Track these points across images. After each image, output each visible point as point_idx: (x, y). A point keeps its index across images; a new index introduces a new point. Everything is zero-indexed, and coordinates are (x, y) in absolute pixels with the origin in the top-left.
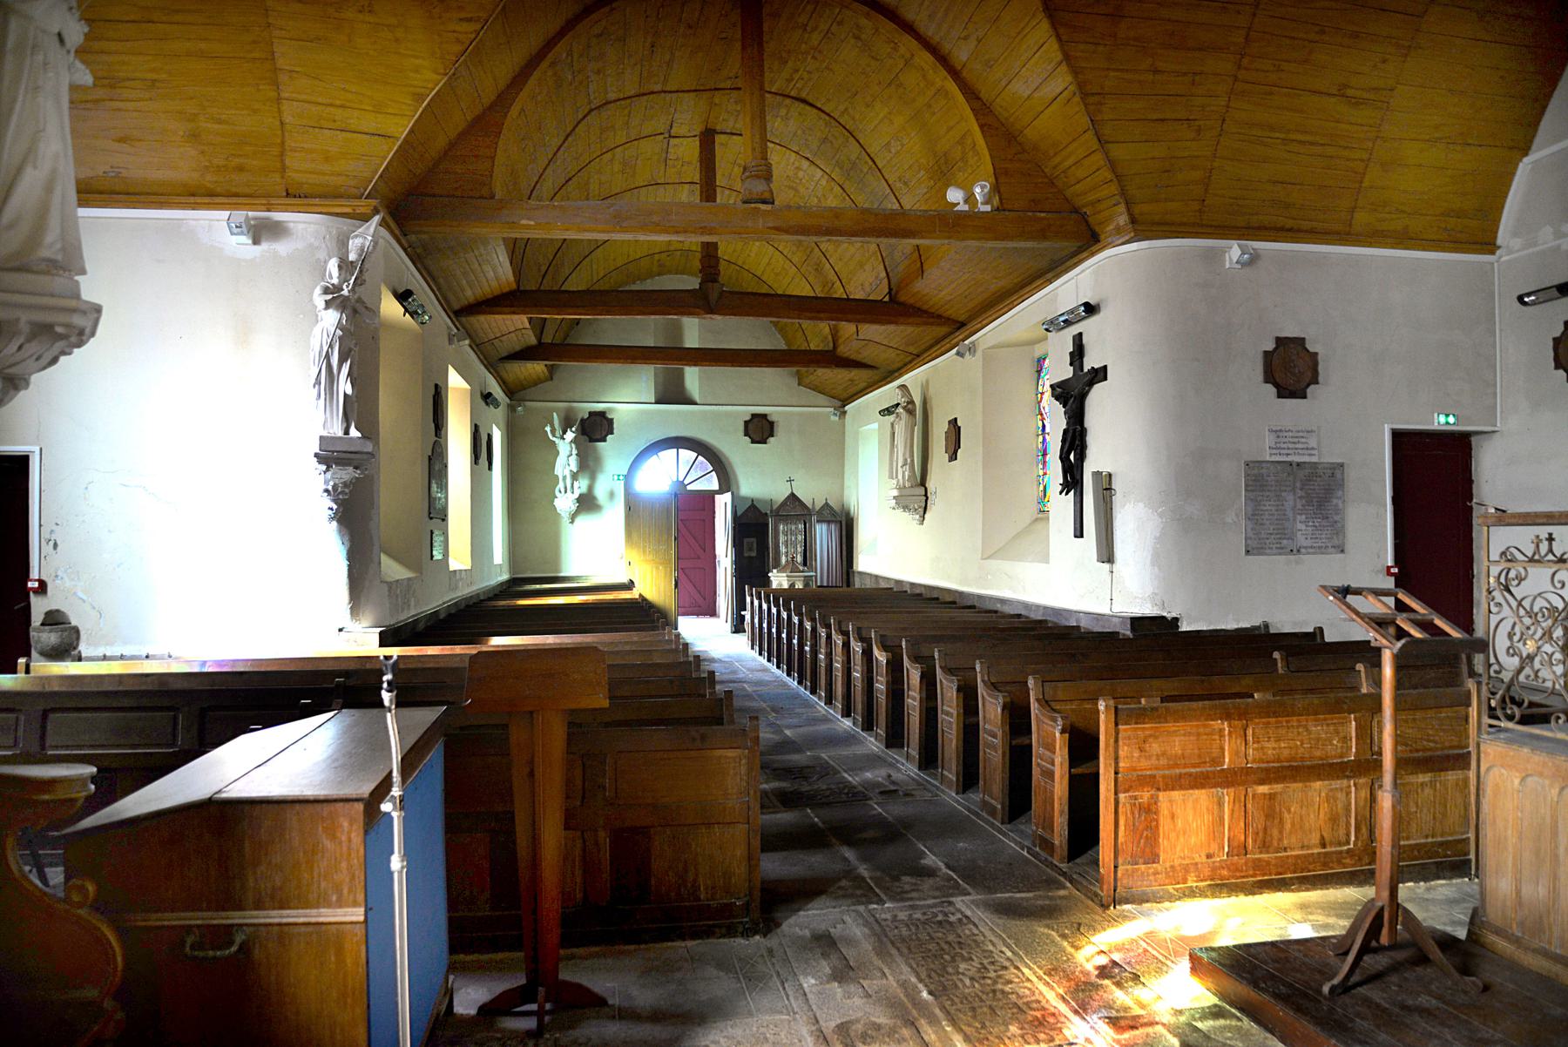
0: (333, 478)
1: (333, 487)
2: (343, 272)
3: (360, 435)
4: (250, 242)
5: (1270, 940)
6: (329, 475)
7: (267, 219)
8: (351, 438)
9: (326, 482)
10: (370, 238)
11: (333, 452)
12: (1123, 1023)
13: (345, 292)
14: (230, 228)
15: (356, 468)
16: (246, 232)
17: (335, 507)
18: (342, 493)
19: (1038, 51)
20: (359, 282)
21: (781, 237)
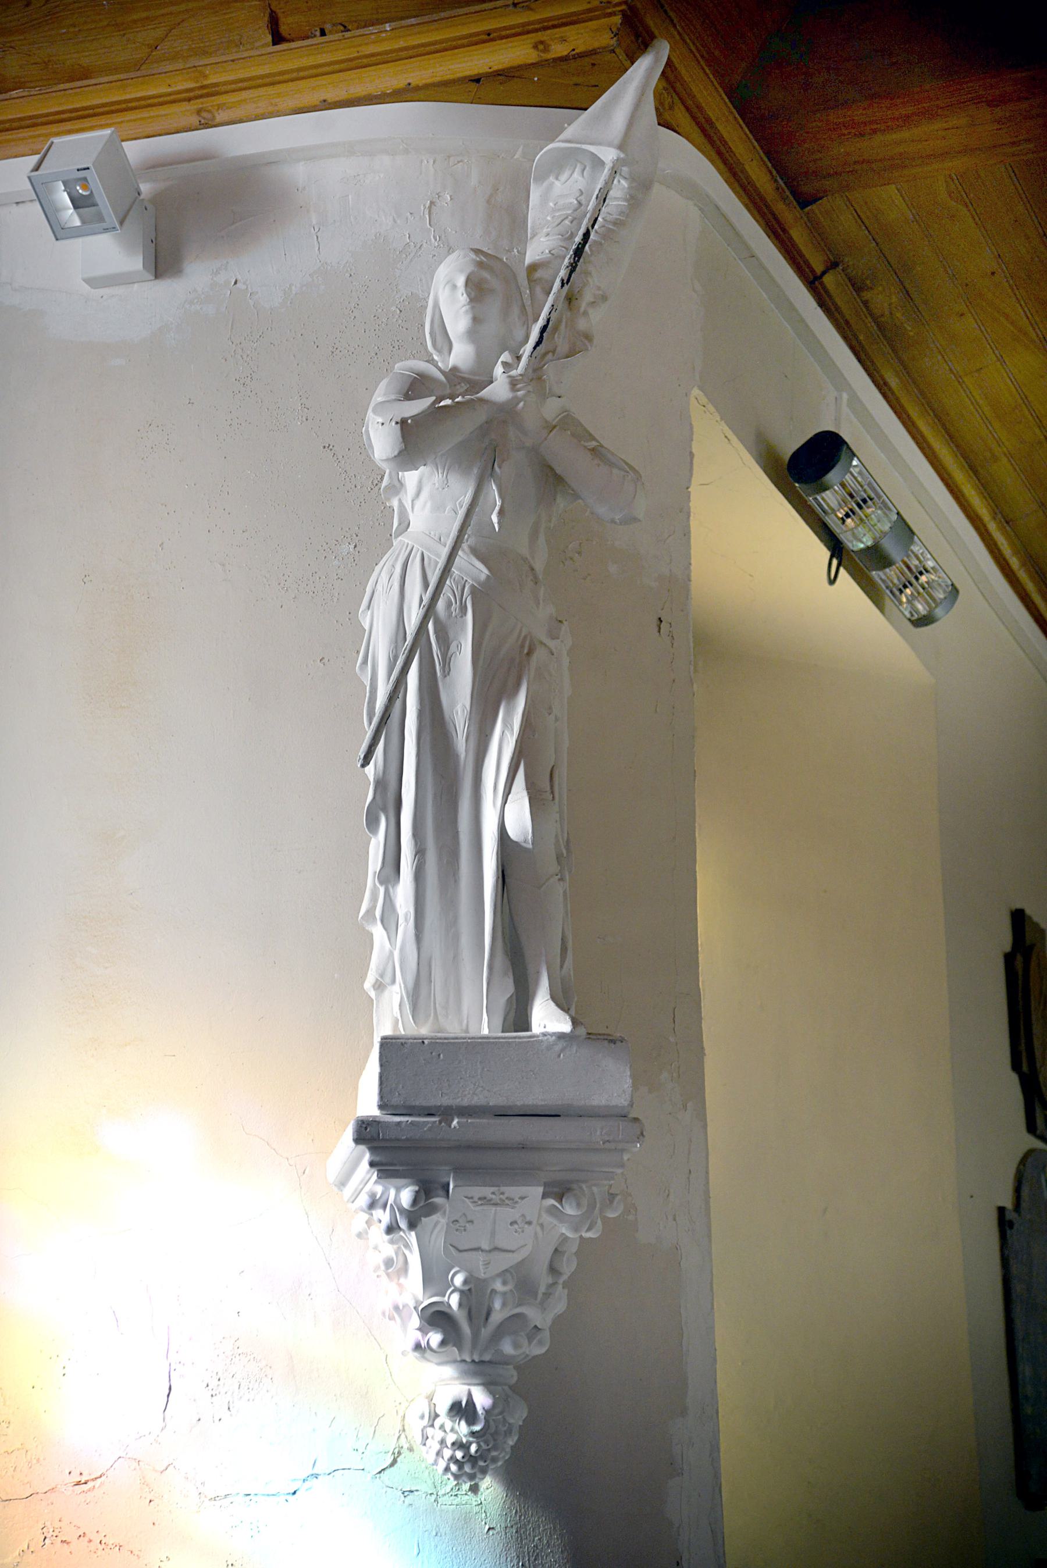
0: (457, 1251)
1: (465, 1294)
2: (493, 307)
3: (565, 1026)
4: (135, 263)
5: (692, 552)
6: (437, 1223)
7: (204, 156)
8: (535, 1043)
9: (432, 1278)
10: (609, 155)
11: (446, 1113)
12: (1019, 960)
13: (498, 390)
14: (51, 215)
15: (559, 1191)
16: (111, 219)
17: (482, 1400)
18: (514, 1324)
19: (100, 84)
20: (561, 341)
21: (20, 135)
